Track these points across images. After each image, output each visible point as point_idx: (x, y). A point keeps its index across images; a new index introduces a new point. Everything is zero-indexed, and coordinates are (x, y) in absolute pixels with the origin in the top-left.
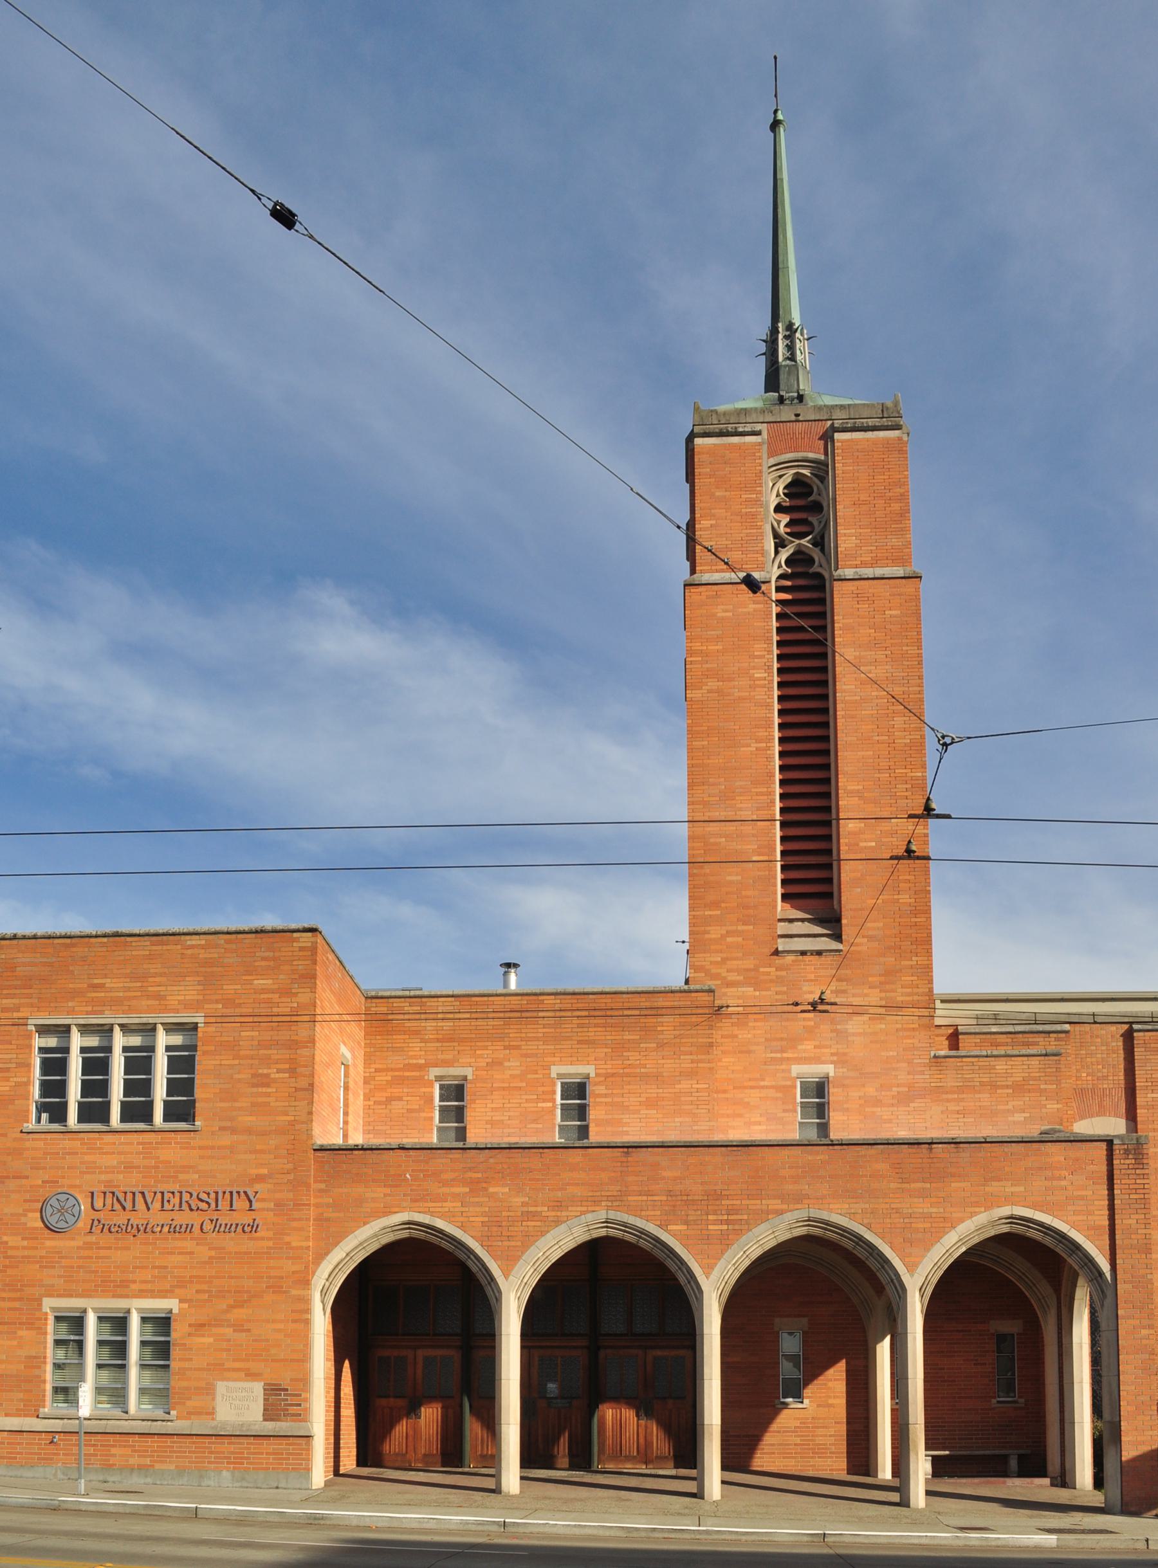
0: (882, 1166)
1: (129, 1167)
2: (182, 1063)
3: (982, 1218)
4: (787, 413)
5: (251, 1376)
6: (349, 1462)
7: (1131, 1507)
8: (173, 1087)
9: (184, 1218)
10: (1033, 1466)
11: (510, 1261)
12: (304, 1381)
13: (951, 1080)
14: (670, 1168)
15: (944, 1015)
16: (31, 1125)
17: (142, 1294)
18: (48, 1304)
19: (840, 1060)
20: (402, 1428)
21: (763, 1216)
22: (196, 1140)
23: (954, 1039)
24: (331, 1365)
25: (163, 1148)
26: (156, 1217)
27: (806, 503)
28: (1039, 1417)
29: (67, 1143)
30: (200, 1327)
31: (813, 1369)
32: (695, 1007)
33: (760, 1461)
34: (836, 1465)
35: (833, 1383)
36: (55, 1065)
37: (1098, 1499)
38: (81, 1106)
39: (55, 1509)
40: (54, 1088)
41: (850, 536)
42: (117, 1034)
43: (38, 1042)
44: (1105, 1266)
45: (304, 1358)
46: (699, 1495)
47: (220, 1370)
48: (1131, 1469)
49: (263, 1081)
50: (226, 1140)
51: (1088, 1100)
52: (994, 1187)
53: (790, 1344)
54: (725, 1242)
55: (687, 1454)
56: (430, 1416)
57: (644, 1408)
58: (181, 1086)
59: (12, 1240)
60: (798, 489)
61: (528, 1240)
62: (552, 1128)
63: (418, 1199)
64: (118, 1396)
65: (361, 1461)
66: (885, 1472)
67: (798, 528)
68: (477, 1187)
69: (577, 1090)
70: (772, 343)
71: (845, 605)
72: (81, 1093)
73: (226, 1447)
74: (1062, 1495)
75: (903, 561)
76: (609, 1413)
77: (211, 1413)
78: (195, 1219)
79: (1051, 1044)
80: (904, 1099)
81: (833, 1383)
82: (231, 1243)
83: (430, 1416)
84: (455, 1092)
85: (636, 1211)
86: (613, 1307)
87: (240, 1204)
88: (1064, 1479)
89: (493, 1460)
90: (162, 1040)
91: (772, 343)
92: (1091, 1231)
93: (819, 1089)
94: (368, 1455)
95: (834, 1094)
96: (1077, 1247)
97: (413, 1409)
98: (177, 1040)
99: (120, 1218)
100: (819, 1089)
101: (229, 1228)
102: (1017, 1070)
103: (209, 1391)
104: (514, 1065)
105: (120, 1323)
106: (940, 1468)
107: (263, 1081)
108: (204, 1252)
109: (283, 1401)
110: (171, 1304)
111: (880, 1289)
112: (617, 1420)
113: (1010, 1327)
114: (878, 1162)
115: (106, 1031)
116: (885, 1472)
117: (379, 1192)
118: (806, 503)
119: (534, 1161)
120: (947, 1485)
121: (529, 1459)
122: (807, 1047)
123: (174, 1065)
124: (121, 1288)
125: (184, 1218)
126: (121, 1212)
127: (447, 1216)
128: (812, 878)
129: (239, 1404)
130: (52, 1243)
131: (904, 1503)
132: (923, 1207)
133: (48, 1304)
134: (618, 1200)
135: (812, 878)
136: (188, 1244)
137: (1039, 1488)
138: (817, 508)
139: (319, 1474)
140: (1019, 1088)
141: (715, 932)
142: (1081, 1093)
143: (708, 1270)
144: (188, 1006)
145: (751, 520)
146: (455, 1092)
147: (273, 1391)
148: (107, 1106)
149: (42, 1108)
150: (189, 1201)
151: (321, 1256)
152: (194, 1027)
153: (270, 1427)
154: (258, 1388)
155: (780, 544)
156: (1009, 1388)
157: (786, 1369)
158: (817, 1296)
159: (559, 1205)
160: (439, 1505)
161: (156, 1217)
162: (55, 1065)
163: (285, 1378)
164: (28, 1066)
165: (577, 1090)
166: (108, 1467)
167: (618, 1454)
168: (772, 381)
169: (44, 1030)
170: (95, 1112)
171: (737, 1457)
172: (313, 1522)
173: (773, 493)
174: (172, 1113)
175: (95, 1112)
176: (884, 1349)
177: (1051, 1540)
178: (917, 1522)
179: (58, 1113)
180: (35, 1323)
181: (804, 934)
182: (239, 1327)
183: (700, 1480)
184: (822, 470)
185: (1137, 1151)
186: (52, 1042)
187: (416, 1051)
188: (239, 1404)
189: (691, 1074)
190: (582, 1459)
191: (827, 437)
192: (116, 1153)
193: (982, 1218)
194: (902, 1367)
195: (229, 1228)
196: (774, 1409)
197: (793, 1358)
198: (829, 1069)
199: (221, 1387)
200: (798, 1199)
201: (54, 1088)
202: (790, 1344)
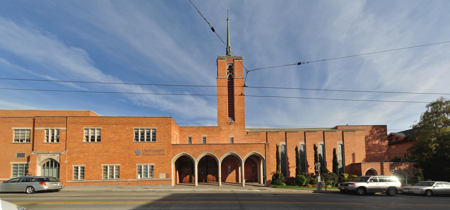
0: (239, 147)
1: (147, 147)
2: (154, 134)
3: (251, 153)
4: (229, 57)
5: (164, 173)
6: (178, 182)
7: (268, 186)
8: (153, 137)
9: (155, 153)
10: (256, 181)
11: (196, 158)
12: (171, 173)
13: (247, 138)
14: (215, 147)
15: (246, 130)
16: (134, 141)
17: (149, 163)
18: (137, 164)
19: (235, 135)
20: (185, 178)
21: (226, 152)
22: (156, 143)
23: (247, 133)
24: (175, 171)
25: (152, 144)
26: (151, 153)
27: (231, 69)
28: (257, 175)
29: (139, 144)
30: (157, 167)
31: (232, 171)
32: (219, 129)
33: (226, 181)
34: (235, 181)
35: (234, 172)
36: (137, 134)
37: (264, 185)
38: (147, 139)
39: (134, 192)
40: (137, 137)
41: (236, 73)
42: (90, 130)
43: (134, 131)
44: (264, 158)
45: (171, 170)
46: (219, 185)
47: (160, 172)
48: (267, 182)
49: (165, 136)
50: (160, 143)
51: (262, 140)
52: (252, 149)
53: (229, 168)
54: (221, 155)
55: (218, 180)
56: (188, 177)
57: (213, 175)
58: (154, 137)
59: (131, 156)
60: (230, 67)
61: (198, 155)
62: (202, 142)
63: (184, 151)
64: (147, 176)
65: (180, 182)
66: (240, 182)
67: (230, 72)
68: (192, 149)
69: (205, 138)
70: (227, 49)
71: (235, 81)
72: (140, 137)
73: (161, 182)
74: (260, 185)
75: (242, 76)
76: (209, 176)
77: (159, 177)
78: (156, 153)
79: (258, 134)
80: (242, 140)
81: (234, 172)
82: (161, 156)
83: (188, 177)
84: (190, 138)
85: (211, 152)
86: (208, 163)
87: (162, 151)
88: (260, 183)
89: (195, 182)
90: (151, 131)
91: (227, 49)
92: (262, 154)
93: (232, 138)
94: (181, 181)
95: (234, 139)
96: (261, 156)
97: (186, 176)
98: (153, 131)
99: (146, 153)
100: (232, 138)
101: (161, 154)
102: (254, 136)
103: (159, 175)
104: (197, 135)
105: (147, 167)
106: (246, 181)
107: (165, 136)
108: (158, 158)
109: (168, 176)
110: (154, 164)
111: (239, 161)
112: (210, 176)
113: (254, 166)
114: (239, 146)
115: (144, 129)
116: (240, 182)
117: (180, 150)
118: (231, 69)
119: (199, 146)
120: (247, 183)
121: (199, 181)
122: (231, 134)
123: (153, 134)
124: (147, 162)
125: (155, 153)
126: (146, 152)
127: (188, 153)
128: (232, 114)
129: (162, 176)
130: (137, 157)
131: (242, 186)
132: (244, 151)
133: (137, 164)
134: (209, 151)
135: (232, 114)
136: (155, 157)
137: (257, 184)
138: (232, 69)
139: (173, 184)
140: (255, 139)
141: (220, 120)
142: (261, 139)
143: (219, 159)
144: (155, 127)
145: (224, 70)
146: (190, 138)
147: (167, 174)
148: (150, 139)
149: (135, 139)
150: (158, 151)
151: (172, 158)
152: (100, 129)
153: (166, 179)
154: (165, 174)
155: (228, 74)
156: (253, 172)
157: (229, 171)
158: (232, 162)
159: (202, 151)
160: (187, 188)
161: (151, 153)
162: (137, 134)
163: (168, 173)
164: (133, 134)
165: (205, 138)
166: (145, 185)
167: (210, 181)
168: (227, 54)
169: (135, 129)
170: (142, 140)
171: (224, 180)
172: (170, 191)
173: (227, 67)
174: (153, 140)
175: (142, 140)
176: (240, 168)
177: (259, 191)
178: (244, 188)
179: (138, 140)
180: (135, 167)
181: (230, 120)
182: (162, 167)
183: (219, 183)
184: (233, 64)
185: (268, 145)
186: (136, 131)
187: (185, 133)
188: (162, 176)
189: (218, 136)
190: (206, 181)
191: (233, 60)
192: (146, 145)
193: (251, 153)
194: (242, 170)
195: (161, 154)
196: (228, 175)
197: (229, 169)
198: (233, 136)
199: (160, 174)
200: (230, 150)
201: (137, 137)
202: (229, 168)
